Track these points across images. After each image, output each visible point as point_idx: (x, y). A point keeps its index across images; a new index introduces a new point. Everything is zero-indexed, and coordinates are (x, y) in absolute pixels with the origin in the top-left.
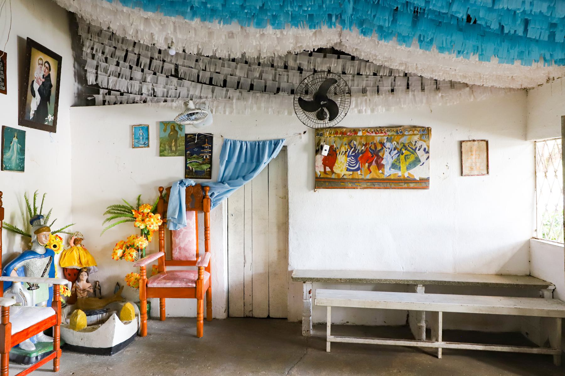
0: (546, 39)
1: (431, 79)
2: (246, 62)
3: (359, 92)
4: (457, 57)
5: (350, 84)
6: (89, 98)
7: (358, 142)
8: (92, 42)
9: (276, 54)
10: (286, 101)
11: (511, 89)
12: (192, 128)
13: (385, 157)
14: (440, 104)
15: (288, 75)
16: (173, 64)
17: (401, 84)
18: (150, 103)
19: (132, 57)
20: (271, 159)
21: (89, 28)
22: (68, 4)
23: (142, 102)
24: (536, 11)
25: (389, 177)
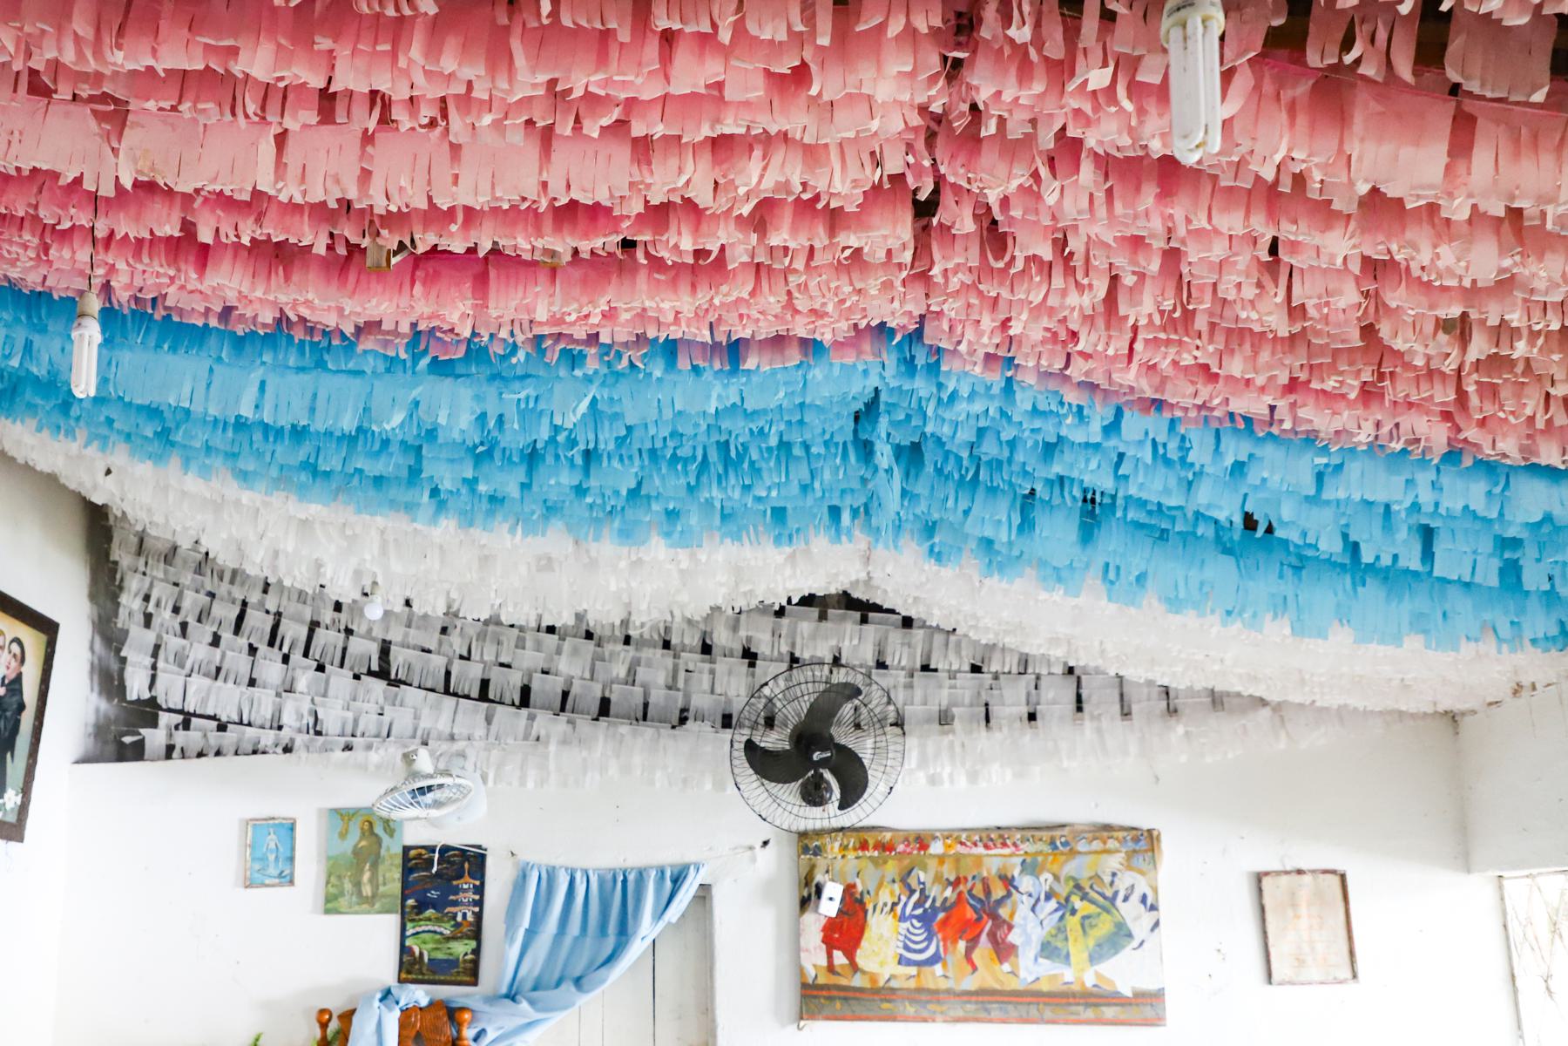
0: (1494, 581)
1: (1150, 683)
2: (589, 635)
3: (928, 721)
4: (1224, 624)
5: (900, 696)
6: (128, 740)
7: (932, 874)
8: (148, 580)
9: (677, 613)
10: (709, 749)
11: (1401, 714)
12: (424, 828)
13: (1017, 920)
14: (1183, 758)
15: (712, 672)
16: (374, 640)
17: (1057, 696)
18: (303, 754)
19: (258, 622)
20: (661, 925)
21: (141, 541)
22: (88, 484)
23: (279, 750)
24: (1451, 505)
25: (1035, 987)
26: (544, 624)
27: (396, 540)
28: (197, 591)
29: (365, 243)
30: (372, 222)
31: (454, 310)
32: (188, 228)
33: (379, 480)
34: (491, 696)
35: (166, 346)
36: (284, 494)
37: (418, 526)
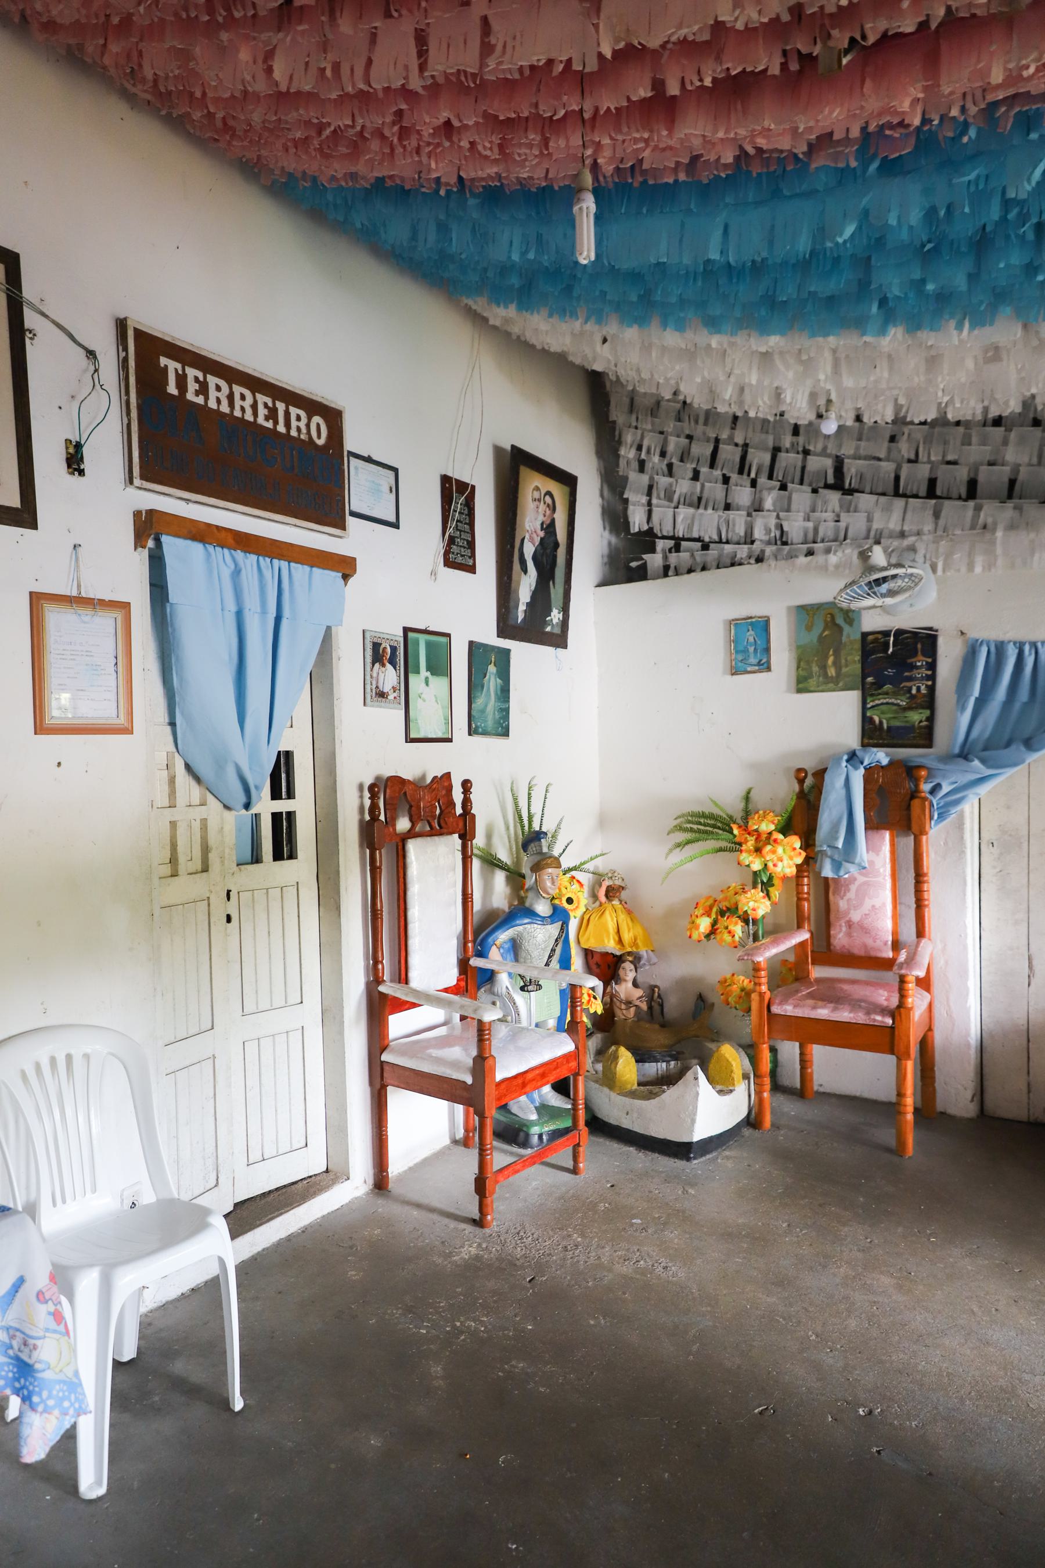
6: (634, 564)
8: (639, 432)
12: (877, 616)
18: (773, 563)
19: (729, 454)
23: (752, 561)
26: (991, 416)
27: (847, 356)
28: (678, 436)
29: (817, 51)
30: (823, 26)
31: (906, 100)
32: (658, 85)
33: (831, 302)
34: (939, 493)
35: (644, 211)
36: (745, 332)
37: (867, 339)
